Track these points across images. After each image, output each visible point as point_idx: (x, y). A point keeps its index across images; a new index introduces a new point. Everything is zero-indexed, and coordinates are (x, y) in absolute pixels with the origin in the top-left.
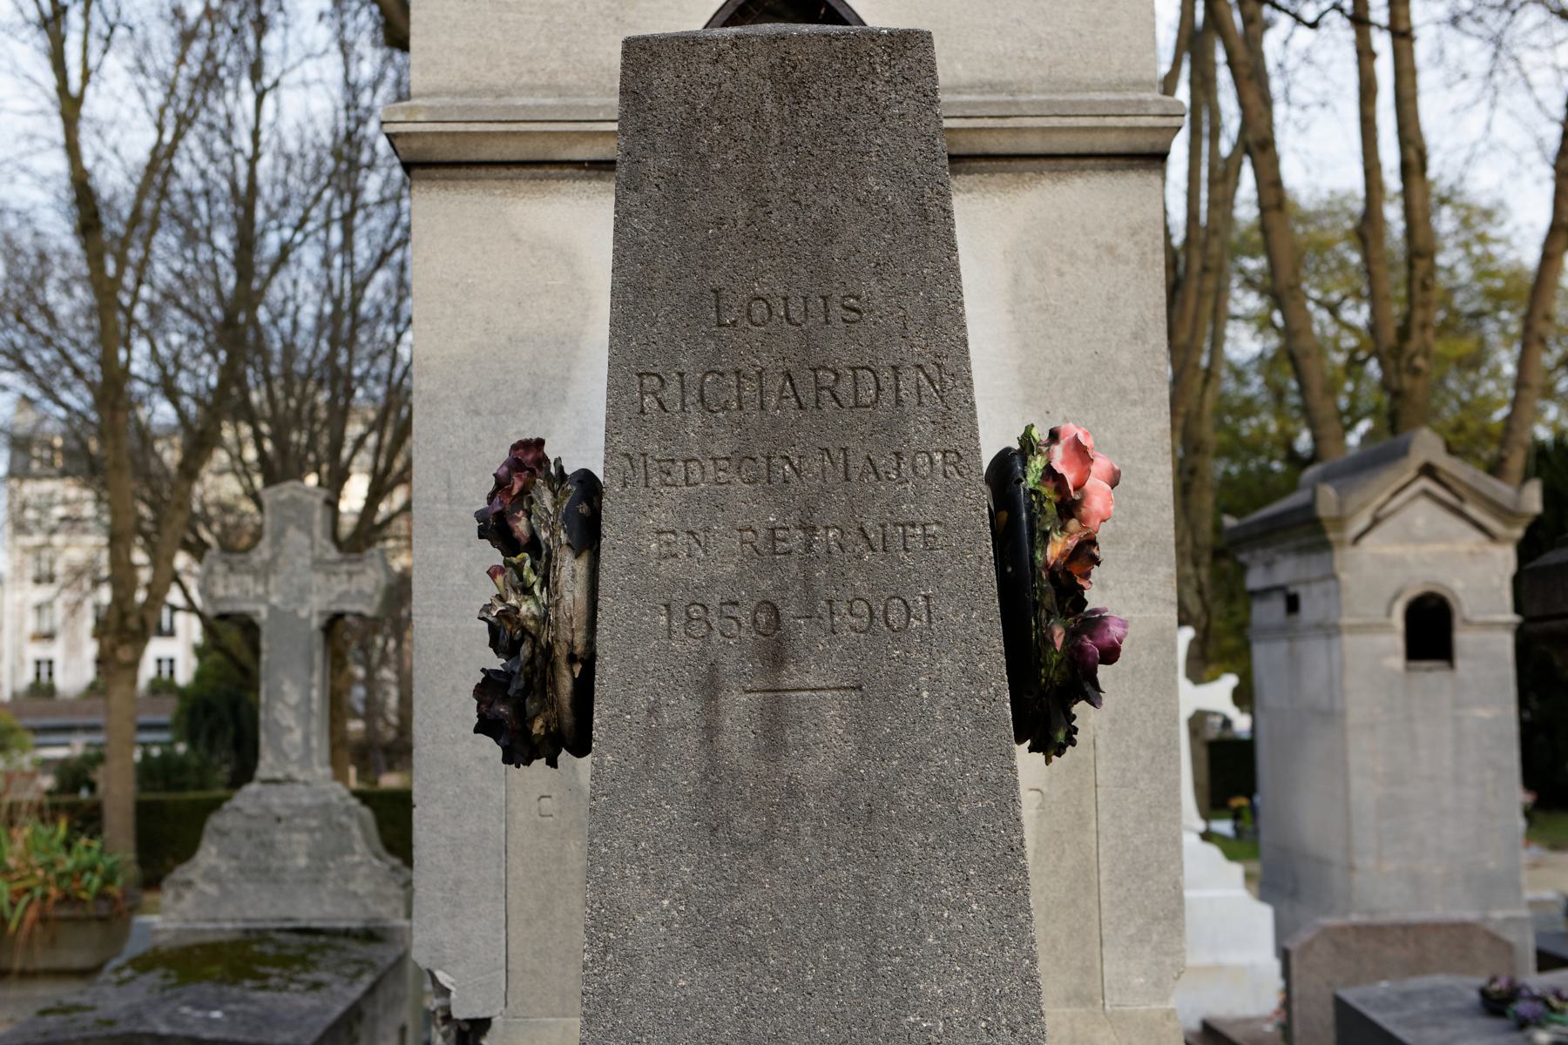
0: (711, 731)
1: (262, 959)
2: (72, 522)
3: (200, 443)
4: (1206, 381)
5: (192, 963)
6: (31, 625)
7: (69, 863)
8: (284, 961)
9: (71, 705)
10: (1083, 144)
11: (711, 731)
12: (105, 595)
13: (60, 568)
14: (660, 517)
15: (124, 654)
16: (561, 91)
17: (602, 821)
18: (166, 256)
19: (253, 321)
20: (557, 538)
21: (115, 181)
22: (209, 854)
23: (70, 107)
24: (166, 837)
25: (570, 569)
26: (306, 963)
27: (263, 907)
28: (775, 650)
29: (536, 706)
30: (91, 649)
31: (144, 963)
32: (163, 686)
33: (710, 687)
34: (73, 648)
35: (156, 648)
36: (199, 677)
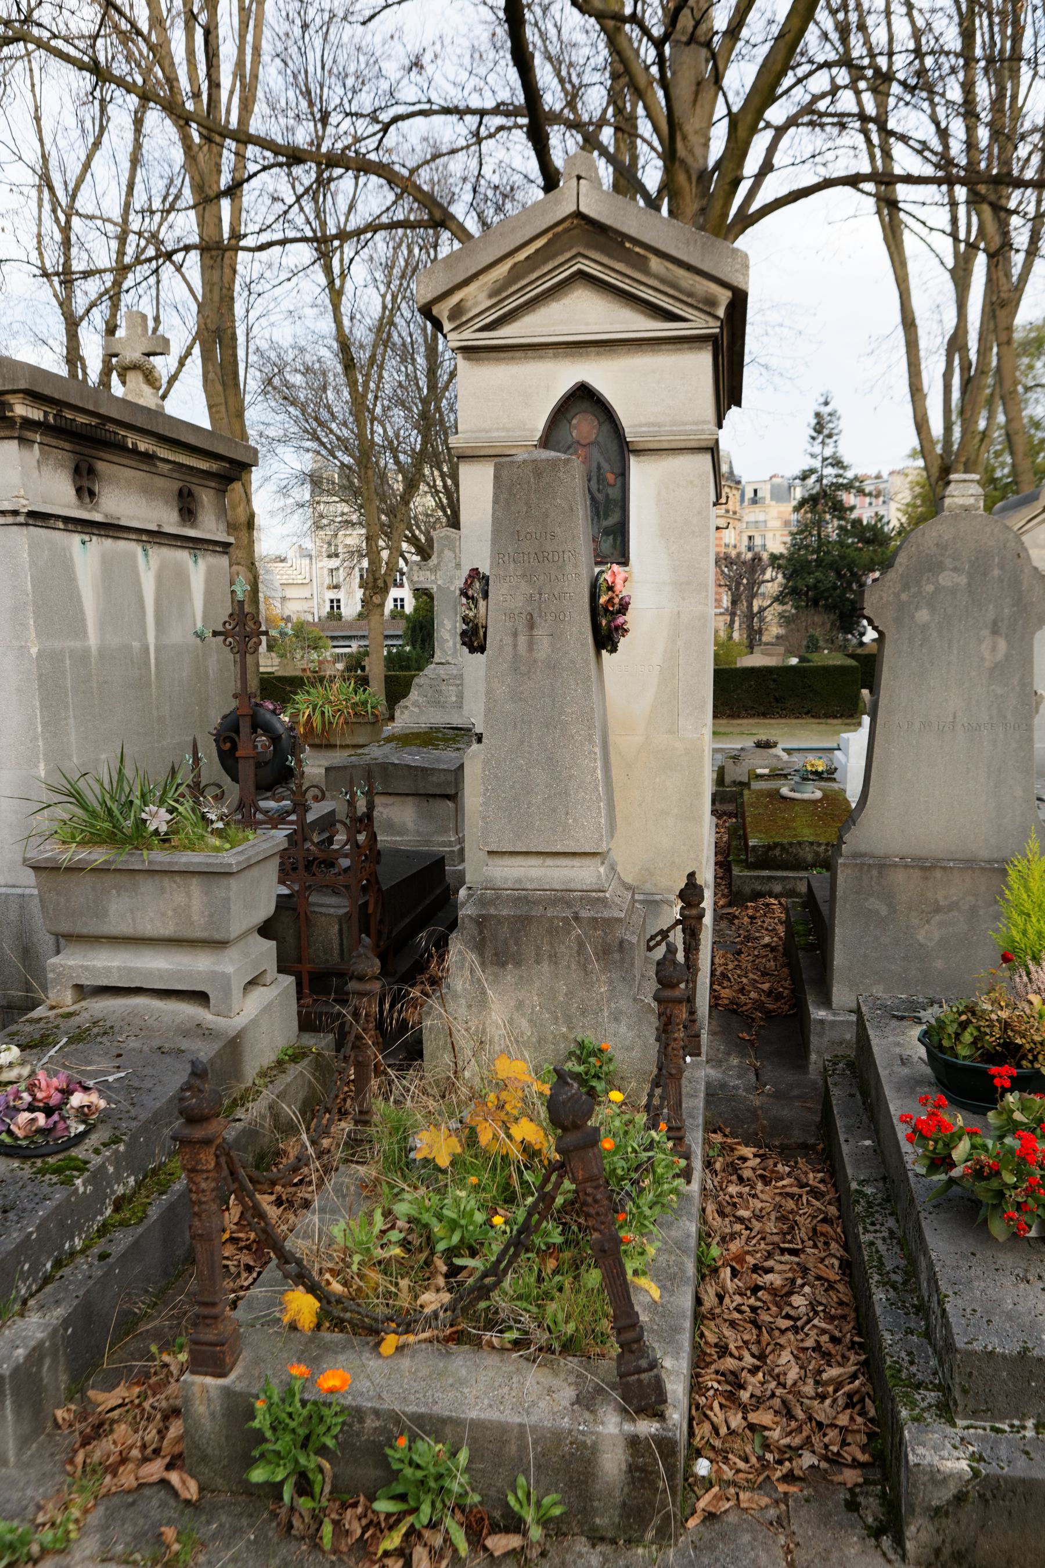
0: (515, 646)
1: (437, 739)
2: (349, 524)
3: (411, 486)
4: (982, 440)
5: (406, 739)
6: (327, 581)
7: (357, 699)
8: (446, 740)
9: (350, 625)
10: (683, 445)
11: (515, 646)
12: (365, 563)
13: (340, 550)
14: (503, 591)
15: (376, 600)
16: (508, 430)
17: (489, 668)
18: (392, 375)
19: (438, 409)
20: (479, 596)
21: (361, 333)
22: (414, 695)
23: (336, 295)
24: (397, 690)
25: (482, 603)
26: (454, 740)
27: (437, 718)
28: (531, 626)
29: (474, 639)
30: (359, 593)
31: (389, 739)
32: (398, 613)
33: (515, 635)
34: (350, 593)
35: (394, 593)
36: (416, 609)
